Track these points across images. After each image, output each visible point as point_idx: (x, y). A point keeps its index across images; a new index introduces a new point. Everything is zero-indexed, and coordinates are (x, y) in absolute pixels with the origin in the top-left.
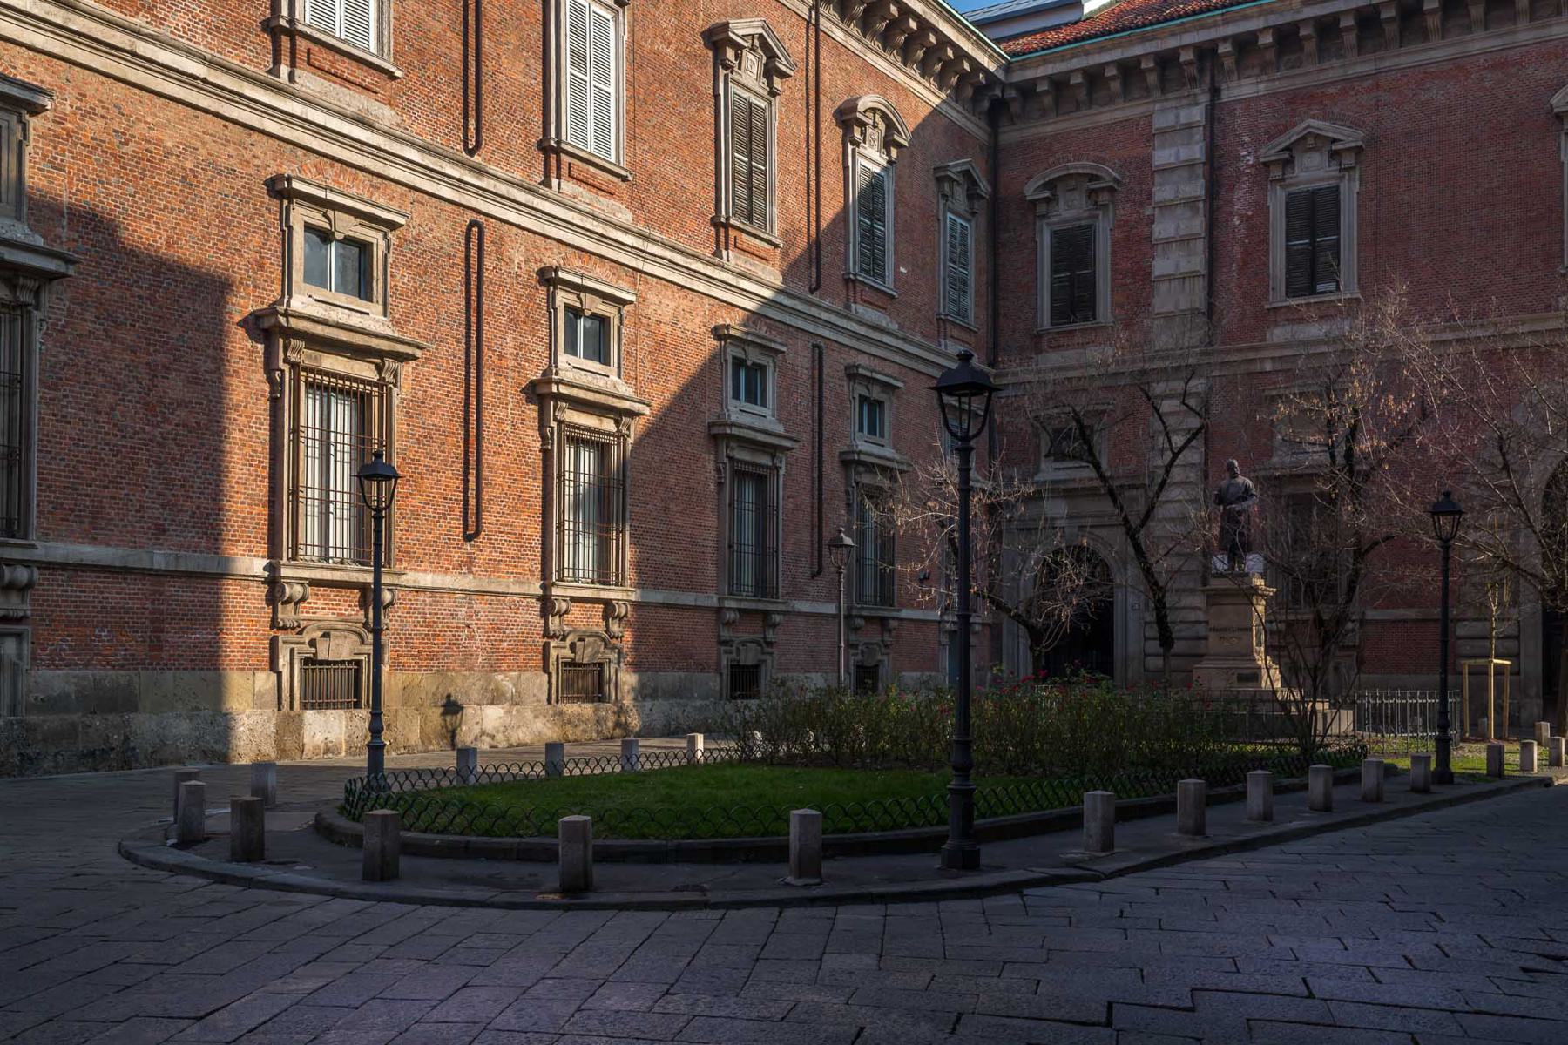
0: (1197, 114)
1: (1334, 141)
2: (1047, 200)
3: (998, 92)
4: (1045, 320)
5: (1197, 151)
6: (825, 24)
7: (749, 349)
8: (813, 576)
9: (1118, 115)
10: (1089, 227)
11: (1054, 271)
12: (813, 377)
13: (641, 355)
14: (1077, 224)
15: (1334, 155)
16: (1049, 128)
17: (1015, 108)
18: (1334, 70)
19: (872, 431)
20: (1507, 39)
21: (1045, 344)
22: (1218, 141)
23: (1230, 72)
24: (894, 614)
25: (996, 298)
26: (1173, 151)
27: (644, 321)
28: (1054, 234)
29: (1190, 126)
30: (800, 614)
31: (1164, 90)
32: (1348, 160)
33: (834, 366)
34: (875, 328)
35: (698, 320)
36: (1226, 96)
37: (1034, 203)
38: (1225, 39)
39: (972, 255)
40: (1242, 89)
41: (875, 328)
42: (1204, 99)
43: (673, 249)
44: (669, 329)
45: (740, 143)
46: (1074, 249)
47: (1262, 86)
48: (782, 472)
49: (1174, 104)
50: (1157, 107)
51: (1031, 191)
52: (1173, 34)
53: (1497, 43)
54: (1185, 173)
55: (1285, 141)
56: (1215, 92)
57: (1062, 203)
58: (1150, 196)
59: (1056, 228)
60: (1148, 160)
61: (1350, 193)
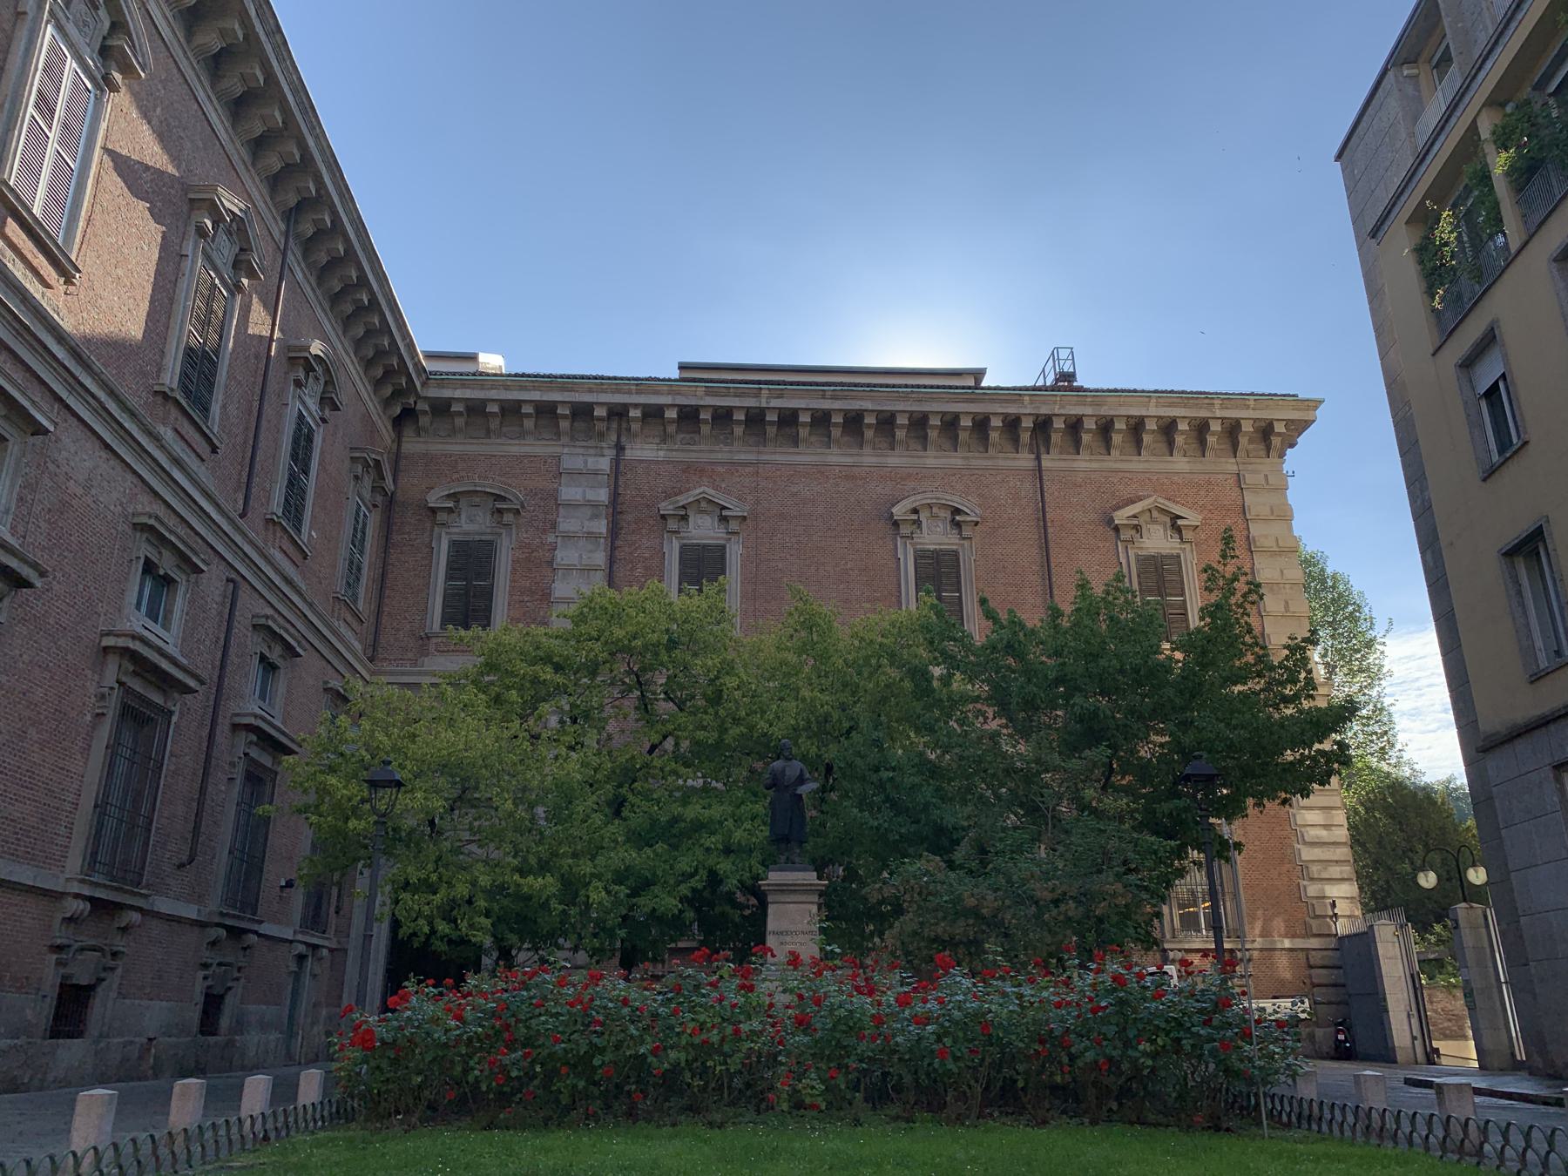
0: (604, 464)
1: (724, 508)
2: (450, 511)
3: (411, 401)
4: (436, 627)
5: (603, 495)
6: (290, 258)
7: (166, 554)
8: (181, 866)
9: (527, 449)
10: (490, 543)
11: (449, 577)
12: (220, 614)
13: (37, 509)
14: (477, 538)
15: (724, 519)
16: (456, 447)
17: (424, 421)
18: (721, 453)
19: (263, 697)
20: (856, 459)
21: (432, 648)
22: (621, 491)
23: (636, 436)
24: (255, 927)
25: (381, 597)
26: (580, 490)
27: (52, 467)
28: (454, 544)
29: (596, 473)
30: (158, 915)
31: (572, 438)
32: (734, 526)
33: (250, 606)
34: (289, 582)
35: (115, 495)
36: (629, 454)
37: (434, 511)
38: (636, 406)
39: (368, 545)
40: (643, 450)
41: (289, 582)
42: (610, 453)
43: (112, 393)
44: (79, 491)
45: (198, 318)
46: (472, 562)
47: (661, 453)
48: (174, 719)
49: (581, 451)
50: (566, 450)
51: (433, 500)
52: (590, 391)
53: (849, 460)
54: (589, 512)
55: (682, 500)
56: (620, 448)
57: (463, 516)
58: (554, 525)
59: (455, 537)
60: (554, 495)
61: (735, 554)
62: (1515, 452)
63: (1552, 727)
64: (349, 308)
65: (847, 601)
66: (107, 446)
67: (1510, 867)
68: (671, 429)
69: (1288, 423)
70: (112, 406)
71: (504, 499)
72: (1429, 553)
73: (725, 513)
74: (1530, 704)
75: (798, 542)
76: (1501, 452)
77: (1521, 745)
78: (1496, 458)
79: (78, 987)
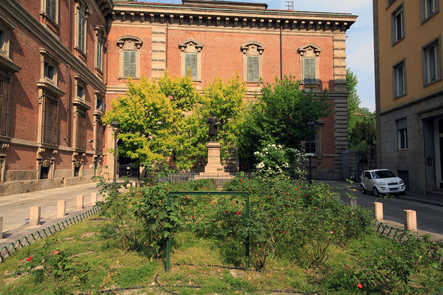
5: (164, 39)
48: (58, 103)
58: (151, 48)
60: (150, 39)
62: (401, 40)
63: (397, 111)
64: (103, 9)
65: (229, 71)
66: (30, 31)
67: (382, 142)
68: (182, 21)
69: (347, 22)
70: (29, 20)
71: (137, 41)
72: (376, 64)
73: (197, 46)
74: (393, 105)
75: (217, 54)
76: (398, 39)
77: (389, 115)
78: (397, 40)
79: (45, 168)
